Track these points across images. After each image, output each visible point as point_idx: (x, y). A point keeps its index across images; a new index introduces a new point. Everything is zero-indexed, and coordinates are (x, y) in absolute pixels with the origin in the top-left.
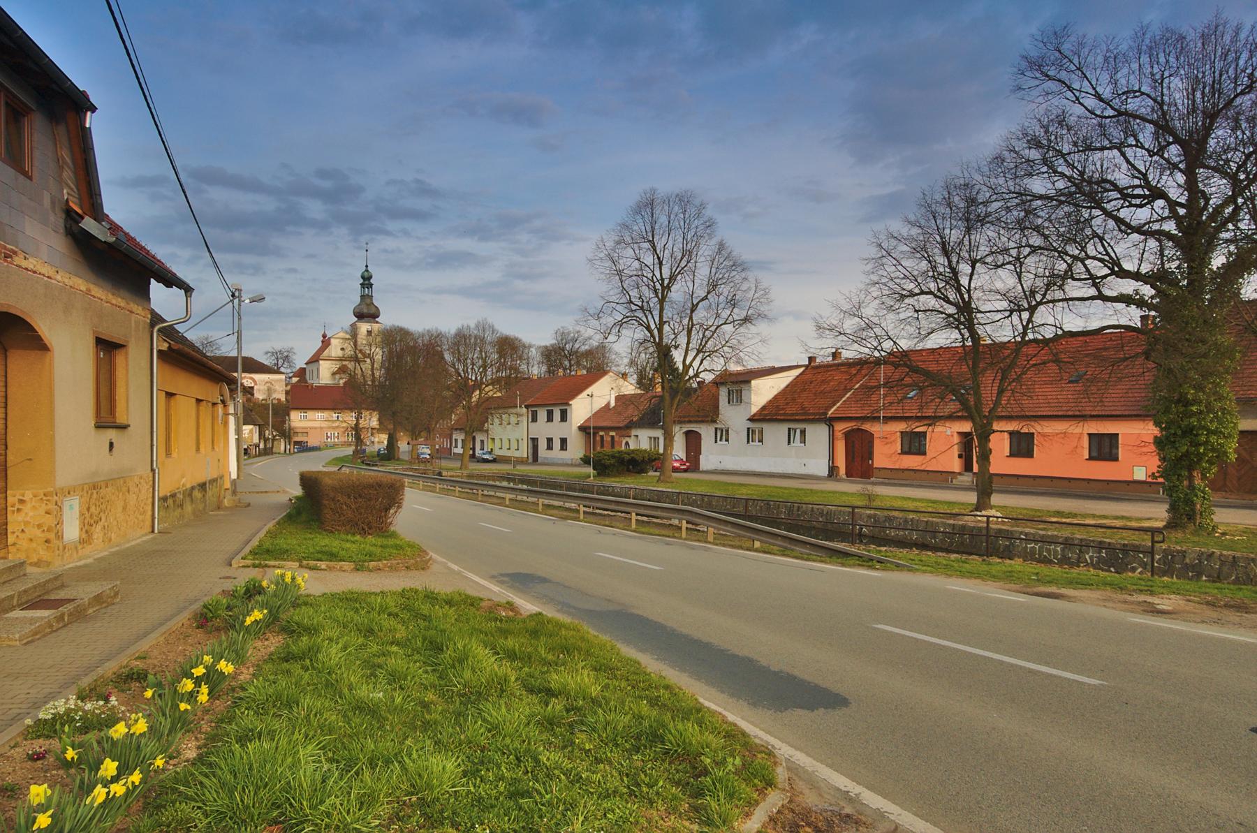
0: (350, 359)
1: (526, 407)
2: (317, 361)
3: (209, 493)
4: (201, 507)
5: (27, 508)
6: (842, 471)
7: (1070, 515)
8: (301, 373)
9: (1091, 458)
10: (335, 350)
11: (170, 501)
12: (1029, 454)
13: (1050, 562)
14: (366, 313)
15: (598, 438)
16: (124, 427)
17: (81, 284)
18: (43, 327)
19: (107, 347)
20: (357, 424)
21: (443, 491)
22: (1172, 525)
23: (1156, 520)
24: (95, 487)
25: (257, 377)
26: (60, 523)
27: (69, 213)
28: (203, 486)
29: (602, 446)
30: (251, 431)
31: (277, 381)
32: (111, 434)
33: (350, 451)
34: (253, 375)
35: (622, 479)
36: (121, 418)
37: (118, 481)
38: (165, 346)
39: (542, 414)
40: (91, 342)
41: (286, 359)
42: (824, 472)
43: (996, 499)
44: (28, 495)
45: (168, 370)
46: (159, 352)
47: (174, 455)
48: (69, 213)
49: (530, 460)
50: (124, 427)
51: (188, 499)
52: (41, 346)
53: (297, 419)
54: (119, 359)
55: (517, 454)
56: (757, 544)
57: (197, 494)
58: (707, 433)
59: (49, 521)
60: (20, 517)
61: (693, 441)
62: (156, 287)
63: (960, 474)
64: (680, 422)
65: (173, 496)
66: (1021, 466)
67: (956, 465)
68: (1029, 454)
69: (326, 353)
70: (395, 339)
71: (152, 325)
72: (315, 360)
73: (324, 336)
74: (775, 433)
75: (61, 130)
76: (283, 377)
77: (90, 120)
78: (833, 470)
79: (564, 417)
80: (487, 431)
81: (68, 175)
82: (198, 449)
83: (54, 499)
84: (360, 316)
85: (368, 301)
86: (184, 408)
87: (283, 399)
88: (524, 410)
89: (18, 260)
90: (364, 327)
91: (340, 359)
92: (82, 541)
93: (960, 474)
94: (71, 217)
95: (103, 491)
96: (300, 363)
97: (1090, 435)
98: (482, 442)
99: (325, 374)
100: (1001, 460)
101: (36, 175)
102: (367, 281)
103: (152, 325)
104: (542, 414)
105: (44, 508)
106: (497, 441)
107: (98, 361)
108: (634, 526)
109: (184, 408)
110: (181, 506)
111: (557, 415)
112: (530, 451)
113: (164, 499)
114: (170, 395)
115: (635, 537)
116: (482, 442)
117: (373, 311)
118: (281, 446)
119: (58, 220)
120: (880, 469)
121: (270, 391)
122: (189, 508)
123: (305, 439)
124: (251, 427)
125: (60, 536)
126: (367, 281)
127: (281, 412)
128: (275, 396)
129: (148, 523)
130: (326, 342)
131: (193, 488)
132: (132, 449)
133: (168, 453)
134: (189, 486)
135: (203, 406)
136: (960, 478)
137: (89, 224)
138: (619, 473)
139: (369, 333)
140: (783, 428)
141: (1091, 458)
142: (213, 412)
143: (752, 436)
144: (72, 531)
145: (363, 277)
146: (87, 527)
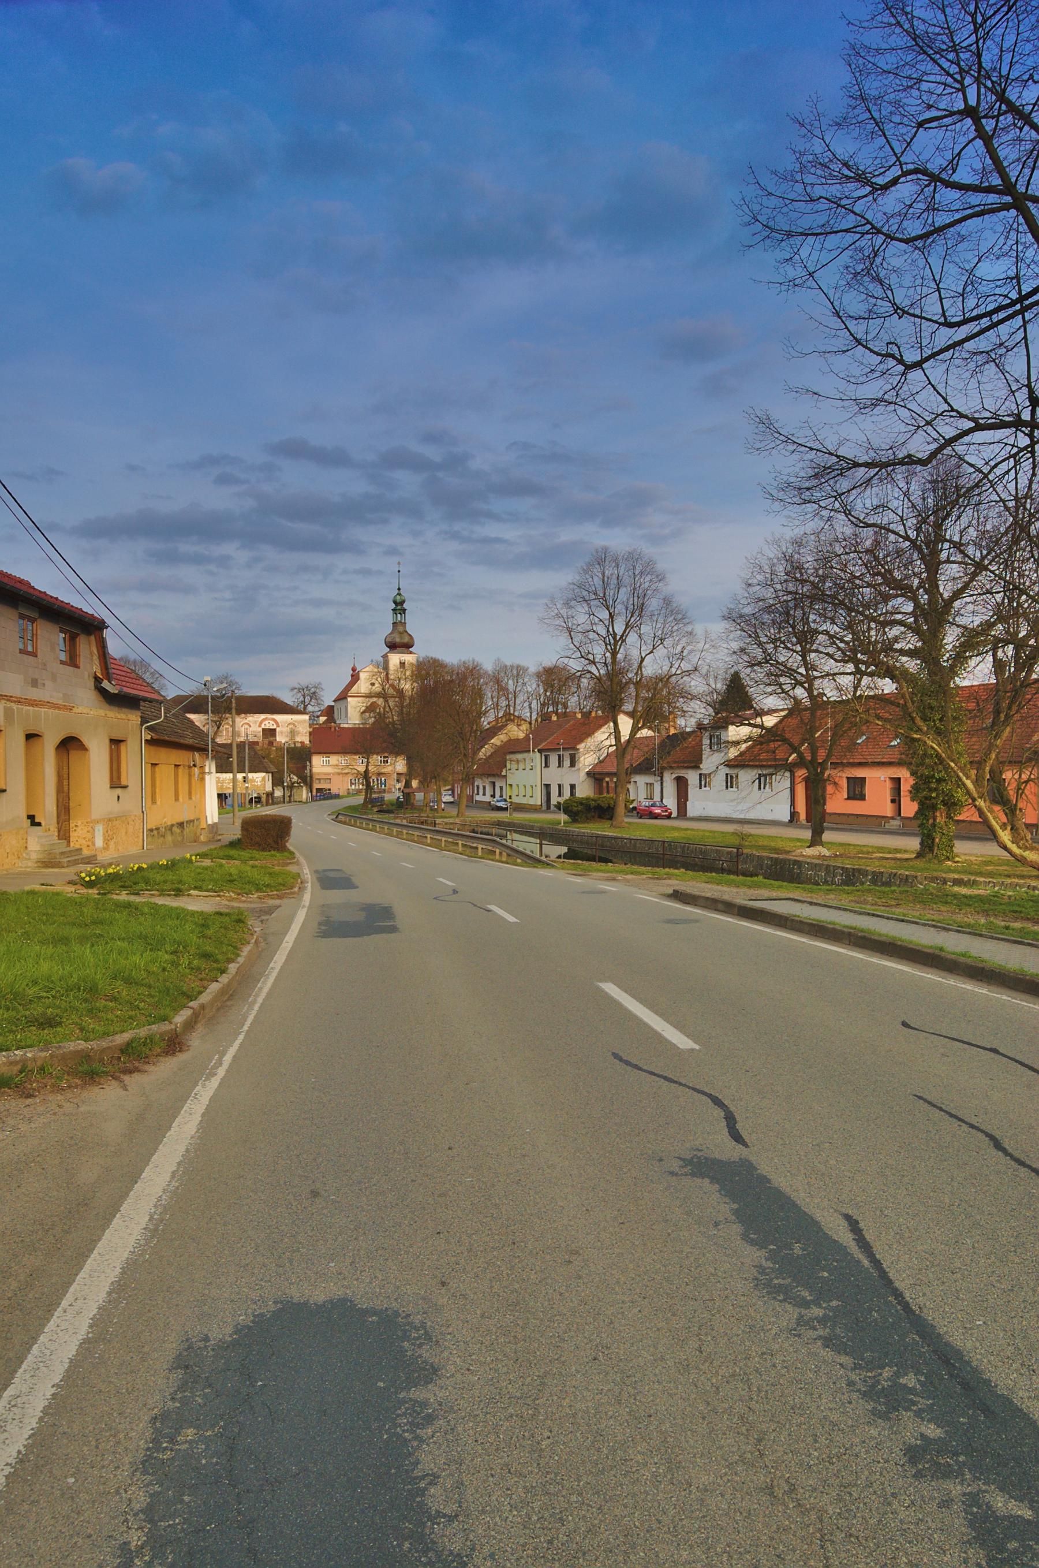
0: (378, 695)
1: (540, 751)
2: (345, 698)
3: (187, 830)
4: (180, 839)
5: (78, 829)
6: (803, 816)
7: (897, 851)
8: (330, 711)
9: (849, 798)
10: (363, 686)
11: (155, 832)
12: (862, 797)
13: (819, 884)
14: (399, 644)
15: (605, 784)
16: (126, 787)
17: (102, 712)
18: (85, 740)
19: (116, 743)
20: (366, 771)
21: (436, 844)
22: (920, 855)
23: (906, 851)
24: (110, 820)
25: (279, 718)
26: (94, 837)
27: (96, 678)
28: (181, 825)
29: (608, 792)
30: (264, 779)
31: (300, 722)
32: (119, 791)
33: (360, 799)
34: (275, 717)
35: (591, 825)
36: (124, 782)
37: (123, 817)
38: (149, 737)
39: (554, 759)
40: (107, 742)
41: (314, 695)
42: (786, 818)
43: (827, 836)
44: (79, 823)
45: (152, 748)
46: (146, 741)
47: (158, 803)
48: (96, 678)
49: (544, 808)
50: (126, 787)
51: (169, 833)
52: (85, 749)
53: (321, 765)
54: (123, 747)
55: (532, 802)
56: (519, 861)
57: (176, 830)
58: (692, 777)
59: (89, 836)
60: (75, 834)
61: (682, 784)
62: (142, 703)
63: (892, 818)
64: (671, 768)
65: (157, 829)
66: (856, 807)
67: (889, 810)
68: (862, 797)
69: (354, 689)
70: (429, 671)
71: (142, 725)
72: (343, 697)
73: (354, 670)
74: (746, 776)
75: (93, 638)
76: (307, 717)
77: (107, 633)
78: (794, 815)
79: (573, 764)
80: (505, 776)
81: (96, 657)
82: (177, 799)
83: (92, 824)
84: (393, 646)
85: (401, 629)
86: (165, 772)
87: (307, 742)
88: (538, 755)
89: (75, 710)
90: (395, 659)
91: (368, 696)
92: (104, 848)
93: (892, 818)
94: (97, 680)
95: (115, 823)
96: (328, 700)
97: (848, 778)
98: (501, 788)
99: (353, 714)
100: (837, 803)
101: (81, 666)
102: (399, 607)
103: (142, 725)
104: (554, 759)
105: (86, 829)
106: (514, 787)
107: (111, 750)
108: (480, 854)
109: (165, 772)
110: (164, 836)
111: (567, 762)
112: (544, 798)
113: (151, 830)
114: (154, 765)
115: (465, 860)
116: (501, 788)
117: (406, 640)
118: (304, 794)
119: (91, 683)
120: (831, 814)
121: (293, 733)
122: (169, 838)
123: (327, 786)
124: (263, 774)
125: (94, 844)
126: (399, 607)
127: (300, 757)
128: (298, 739)
129: (141, 843)
130: (355, 678)
131: (172, 825)
132: (130, 801)
133: (154, 802)
134: (169, 823)
135: (181, 769)
136: (892, 822)
137: (105, 684)
138: (588, 820)
139: (402, 664)
140: (754, 773)
141: (849, 798)
142: (190, 776)
143: (730, 782)
144: (99, 842)
145: (395, 602)
146: (107, 840)
